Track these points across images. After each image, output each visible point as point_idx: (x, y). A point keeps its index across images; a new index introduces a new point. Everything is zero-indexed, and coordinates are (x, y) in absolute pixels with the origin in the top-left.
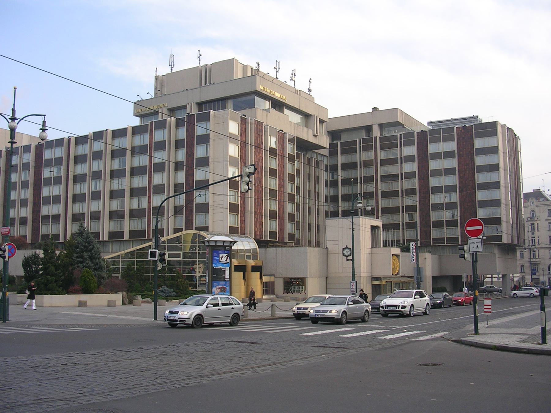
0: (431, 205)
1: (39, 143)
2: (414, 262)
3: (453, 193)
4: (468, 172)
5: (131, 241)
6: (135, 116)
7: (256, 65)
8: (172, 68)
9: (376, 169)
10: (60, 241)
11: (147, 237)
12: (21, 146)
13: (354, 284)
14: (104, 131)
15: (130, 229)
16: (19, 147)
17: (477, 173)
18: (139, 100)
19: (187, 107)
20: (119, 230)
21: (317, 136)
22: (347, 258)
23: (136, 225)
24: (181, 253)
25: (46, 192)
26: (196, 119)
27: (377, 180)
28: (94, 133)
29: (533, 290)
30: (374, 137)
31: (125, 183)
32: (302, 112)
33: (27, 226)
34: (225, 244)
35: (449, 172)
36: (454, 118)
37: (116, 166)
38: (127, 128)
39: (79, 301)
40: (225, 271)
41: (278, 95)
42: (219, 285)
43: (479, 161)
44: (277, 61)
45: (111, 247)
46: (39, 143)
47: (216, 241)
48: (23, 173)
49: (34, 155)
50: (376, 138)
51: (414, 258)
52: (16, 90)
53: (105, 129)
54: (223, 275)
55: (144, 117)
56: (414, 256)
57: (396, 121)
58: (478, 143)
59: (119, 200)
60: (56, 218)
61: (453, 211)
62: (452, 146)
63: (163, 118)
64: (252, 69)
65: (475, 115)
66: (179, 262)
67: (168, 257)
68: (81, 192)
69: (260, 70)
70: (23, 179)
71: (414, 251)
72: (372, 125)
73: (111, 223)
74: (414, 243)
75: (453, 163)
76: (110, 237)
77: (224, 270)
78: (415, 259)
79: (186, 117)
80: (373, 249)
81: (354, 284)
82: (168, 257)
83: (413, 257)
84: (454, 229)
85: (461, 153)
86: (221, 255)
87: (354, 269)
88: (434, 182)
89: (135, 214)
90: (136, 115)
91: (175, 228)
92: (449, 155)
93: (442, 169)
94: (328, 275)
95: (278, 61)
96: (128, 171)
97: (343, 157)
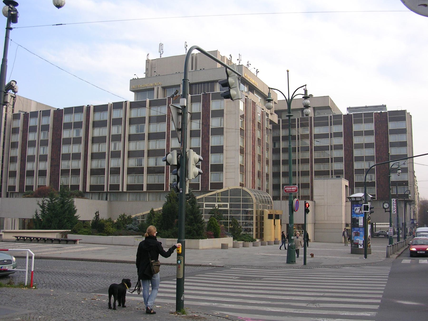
0: (354, 170)
2: (395, 213)
3: (372, 161)
4: (382, 147)
6: (131, 91)
7: (230, 57)
8: (161, 54)
9: (311, 141)
10: (16, 191)
11: (165, 190)
12: (39, 111)
13: (392, 229)
14: (124, 103)
15: (147, 183)
16: (38, 111)
17: (390, 147)
18: (134, 78)
20: (116, 183)
21: (273, 114)
22: (385, 210)
23: (154, 179)
24: (228, 204)
25: (65, 150)
27: (312, 150)
28: (114, 103)
30: (310, 117)
32: (263, 94)
33: (16, 178)
34: (357, 199)
35: (368, 146)
36: (368, 105)
38: (108, 105)
39: (222, 244)
40: (358, 220)
41: (253, 81)
42: (354, 230)
43: (392, 138)
44: (239, 55)
45: (128, 198)
47: (355, 198)
48: (42, 134)
49: (53, 119)
50: (311, 118)
51: (395, 210)
52: (289, 72)
53: (125, 101)
54: (357, 223)
55: (138, 92)
56: (395, 209)
57: (327, 106)
58: (391, 126)
60: (76, 172)
61: (371, 175)
62: (371, 127)
64: (227, 59)
65: (384, 104)
66: (226, 212)
68: (99, 151)
69: (232, 61)
70: (42, 138)
71: (395, 205)
73: (92, 178)
74: (394, 199)
75: (371, 139)
76: (148, 189)
77: (358, 219)
78: (396, 211)
79: (202, 95)
80: (347, 203)
81: (392, 229)
83: (394, 209)
84: (372, 189)
85: (378, 132)
86: (355, 208)
87: (391, 218)
88: (357, 153)
89: (152, 171)
91: (190, 183)
92: (368, 133)
93: (363, 144)
94: (315, 222)
95: (240, 54)
97: (284, 131)
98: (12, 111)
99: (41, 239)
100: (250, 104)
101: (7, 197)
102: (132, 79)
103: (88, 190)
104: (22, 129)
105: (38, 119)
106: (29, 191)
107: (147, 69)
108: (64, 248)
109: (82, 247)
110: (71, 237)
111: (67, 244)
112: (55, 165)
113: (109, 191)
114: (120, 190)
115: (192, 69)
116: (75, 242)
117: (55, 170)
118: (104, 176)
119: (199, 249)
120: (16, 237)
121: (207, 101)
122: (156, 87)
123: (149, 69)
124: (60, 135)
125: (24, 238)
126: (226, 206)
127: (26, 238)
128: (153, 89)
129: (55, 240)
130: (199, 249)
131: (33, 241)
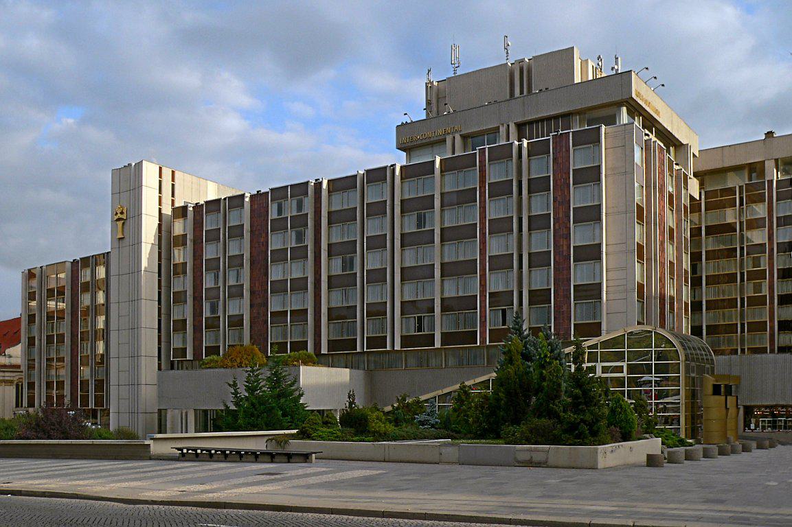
1: (258, 192)
5: (366, 355)
19: (501, 129)
24: (625, 365)
25: (275, 273)
26: (571, 141)
27: (772, 250)
28: (368, 171)
29: (173, 417)
30: (768, 181)
31: (436, 255)
37: (411, 228)
46: (258, 192)
59: (420, 284)
63: (509, 141)
66: (620, 382)
67: (602, 373)
72: (764, 161)
79: (551, 137)
82: (602, 373)
90: (401, 147)
96: (438, 234)
98: (170, 203)
99: (246, 453)
100: (655, 151)
101: (172, 368)
102: (400, 124)
103: (324, 351)
104: (192, 238)
105: (221, 215)
106: (211, 357)
107: (428, 103)
108: (282, 476)
109: (324, 469)
110: (297, 446)
111: (289, 462)
112: (259, 303)
113: (365, 350)
114: (388, 348)
115: (522, 92)
116: (306, 457)
117: (258, 313)
118: (432, 176)
119: (597, 469)
120: (179, 449)
121: (564, 150)
122: (451, 136)
123: (434, 101)
124: (264, 243)
125: (182, 451)
126: (620, 369)
127: (213, 452)
128: (445, 141)
129: (263, 453)
130: (597, 469)
131: (260, 458)
